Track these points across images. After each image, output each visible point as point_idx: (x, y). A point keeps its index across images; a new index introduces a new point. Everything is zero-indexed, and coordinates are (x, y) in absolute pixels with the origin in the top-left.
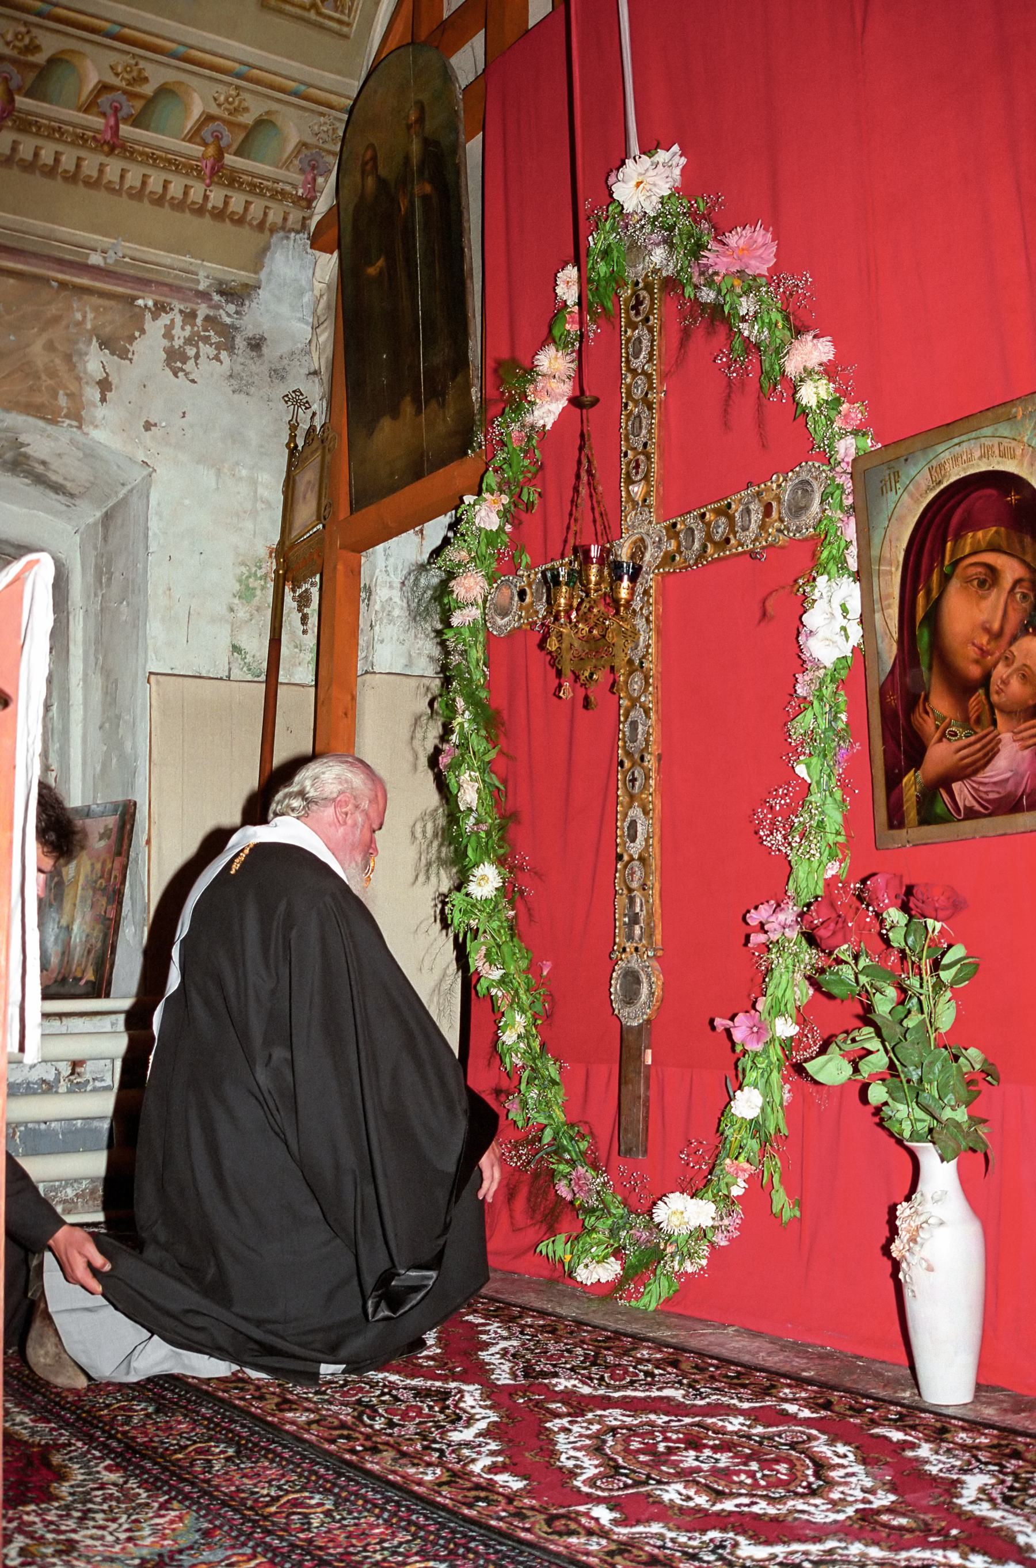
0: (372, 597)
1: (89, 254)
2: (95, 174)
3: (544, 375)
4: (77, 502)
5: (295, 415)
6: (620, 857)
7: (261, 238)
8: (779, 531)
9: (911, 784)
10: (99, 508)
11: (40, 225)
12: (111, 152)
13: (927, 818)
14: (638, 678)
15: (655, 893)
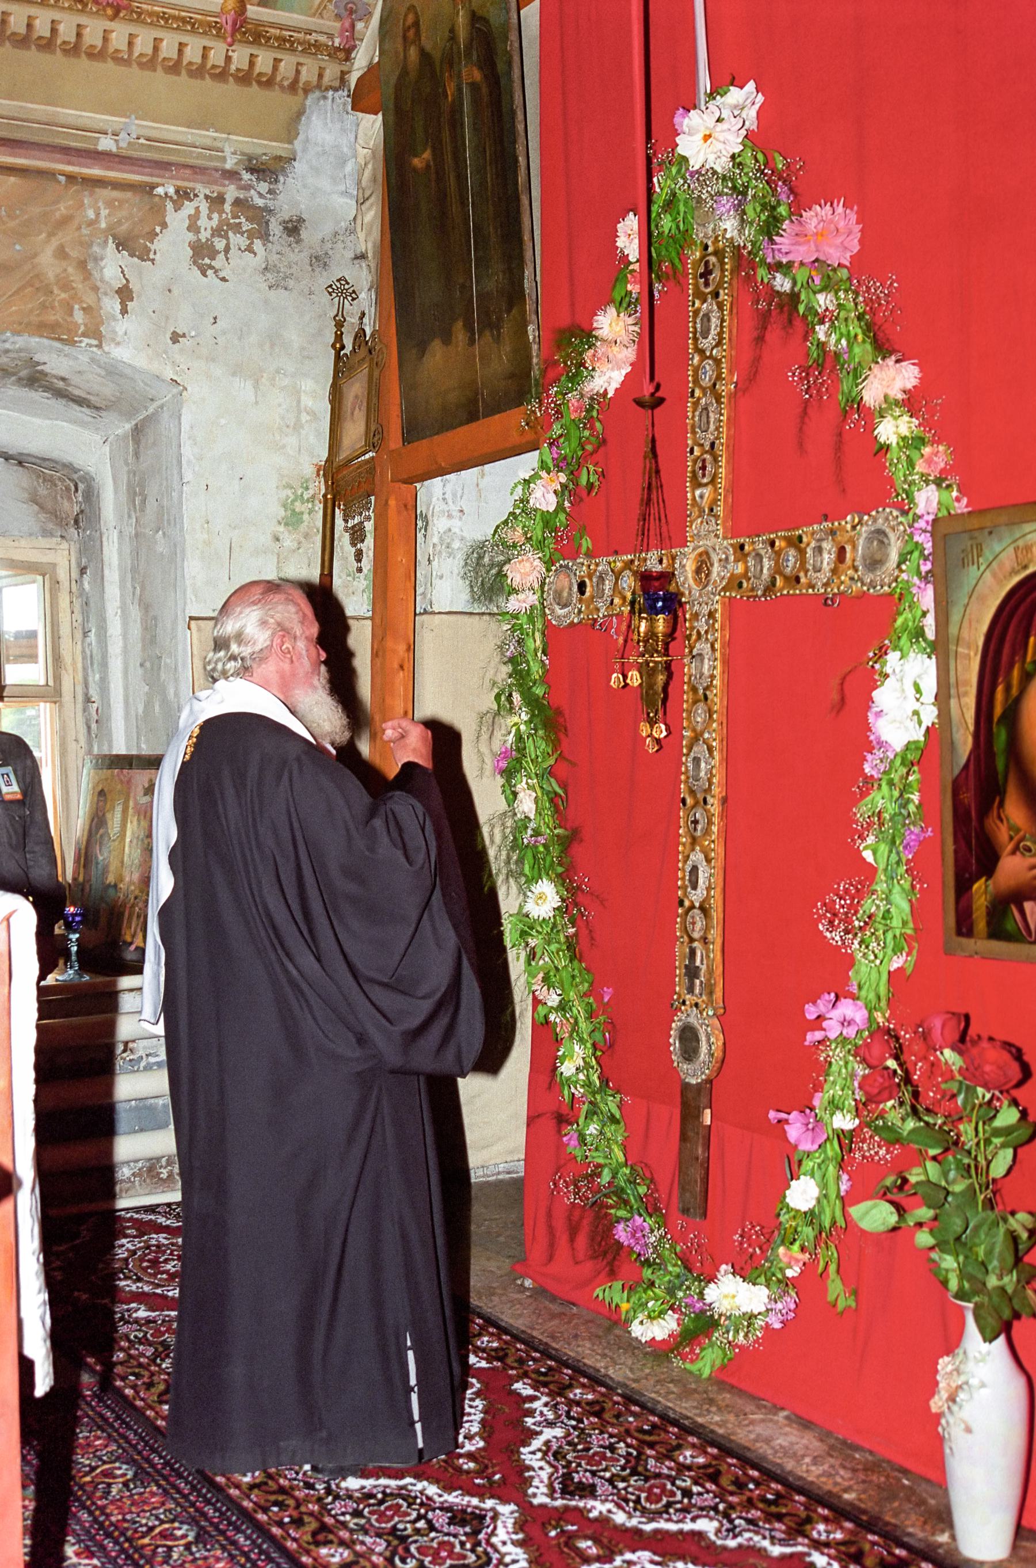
0: (429, 528)
1: (98, 138)
2: (99, 43)
3: (603, 340)
4: (104, 414)
5: (341, 309)
6: (681, 903)
7: (292, 101)
8: (852, 579)
9: (981, 891)
10: (128, 421)
11: (39, 109)
12: (115, 16)
13: (997, 932)
14: (701, 708)
15: (716, 948)
